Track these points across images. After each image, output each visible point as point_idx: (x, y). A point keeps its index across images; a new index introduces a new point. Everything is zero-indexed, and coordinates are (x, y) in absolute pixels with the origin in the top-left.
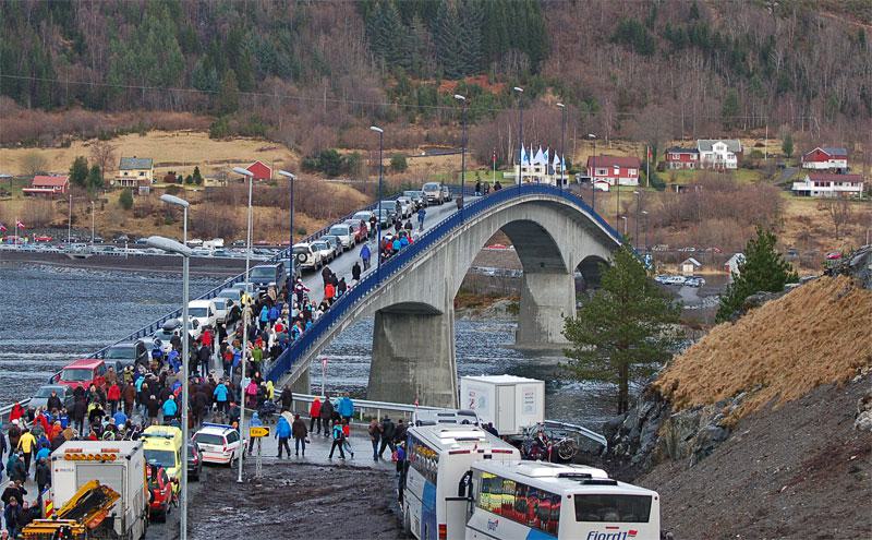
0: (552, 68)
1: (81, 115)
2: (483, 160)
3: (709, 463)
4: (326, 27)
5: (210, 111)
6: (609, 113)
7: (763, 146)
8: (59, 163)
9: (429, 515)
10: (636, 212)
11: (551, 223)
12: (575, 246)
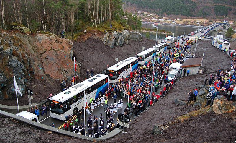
0: (228, 16)
1: (195, 17)
2: (222, 22)
3: (234, 42)
4: (212, 12)
5: (203, 17)
6: (231, 18)
7: (20, 134)
8: (193, 21)
9: (214, 43)
10: (232, 26)
11: (226, 26)
12: (227, 27)
